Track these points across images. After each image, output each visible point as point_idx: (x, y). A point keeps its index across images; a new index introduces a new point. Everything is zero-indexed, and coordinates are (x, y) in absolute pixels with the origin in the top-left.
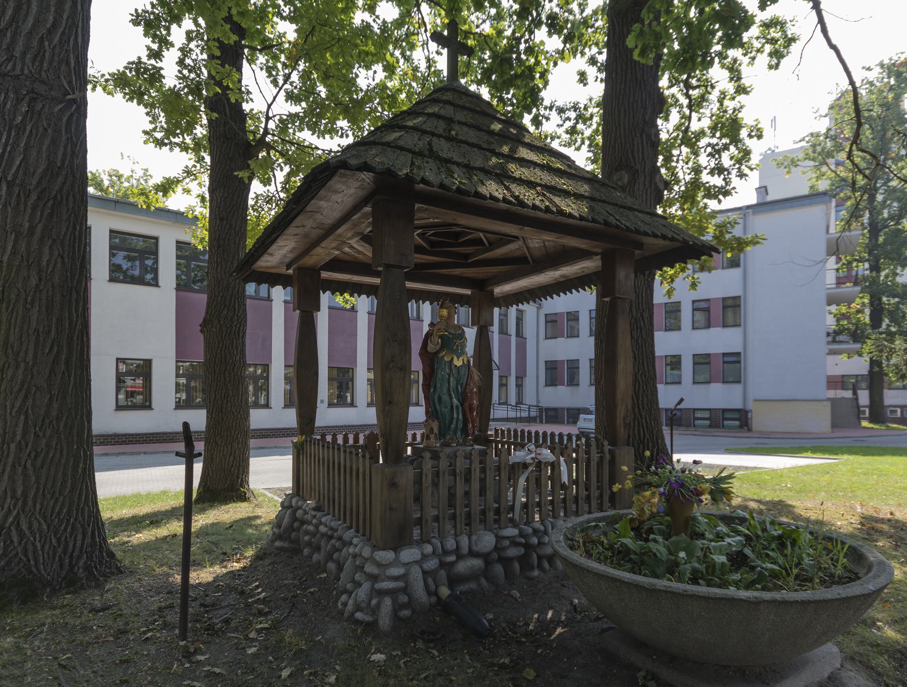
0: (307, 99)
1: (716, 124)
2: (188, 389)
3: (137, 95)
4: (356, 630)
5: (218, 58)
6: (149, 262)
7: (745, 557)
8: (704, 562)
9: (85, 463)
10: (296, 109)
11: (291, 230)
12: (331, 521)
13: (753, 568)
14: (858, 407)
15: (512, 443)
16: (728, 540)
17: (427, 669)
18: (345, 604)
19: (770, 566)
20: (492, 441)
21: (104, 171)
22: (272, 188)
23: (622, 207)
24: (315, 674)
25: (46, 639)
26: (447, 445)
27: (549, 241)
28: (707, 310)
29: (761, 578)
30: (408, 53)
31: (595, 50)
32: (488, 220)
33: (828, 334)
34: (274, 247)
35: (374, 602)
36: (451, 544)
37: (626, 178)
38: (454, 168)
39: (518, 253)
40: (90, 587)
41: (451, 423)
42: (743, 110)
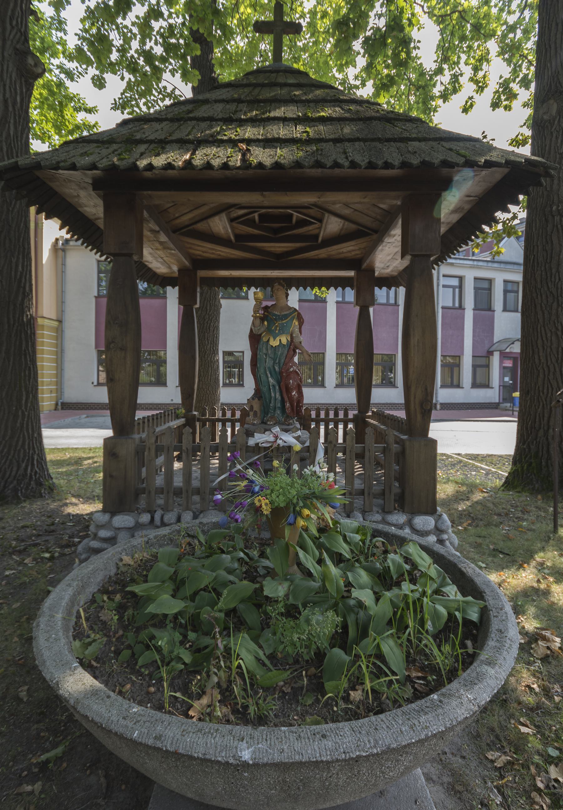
41: (270, 402)
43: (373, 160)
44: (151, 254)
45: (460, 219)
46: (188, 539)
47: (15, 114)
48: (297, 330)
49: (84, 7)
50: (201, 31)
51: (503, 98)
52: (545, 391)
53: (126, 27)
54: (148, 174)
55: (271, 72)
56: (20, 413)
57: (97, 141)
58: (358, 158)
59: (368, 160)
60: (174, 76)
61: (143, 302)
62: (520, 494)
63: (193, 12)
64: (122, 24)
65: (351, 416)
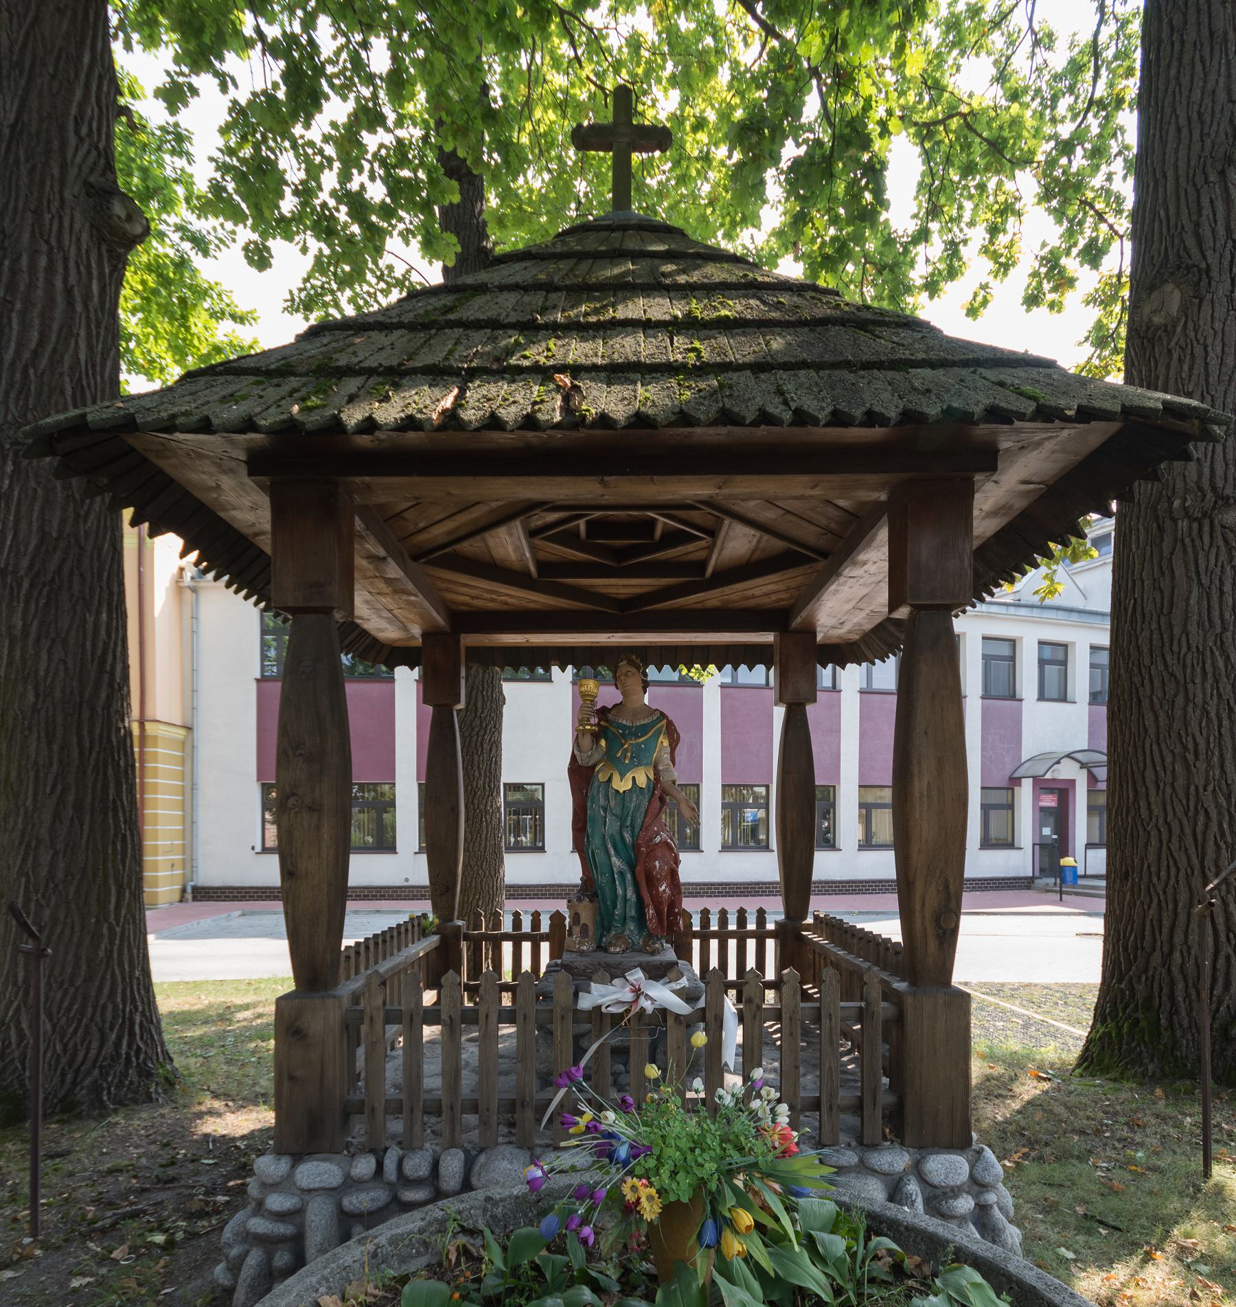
32: (754, 478)
41: (615, 907)
43: (843, 406)
44: (367, 602)
45: (1002, 529)
46: (462, 1240)
47: (88, 317)
48: (667, 756)
49: (224, 102)
50: (461, 153)
51: (1047, 286)
52: (1163, 874)
53: (311, 144)
54: (364, 440)
55: (610, 228)
56: (105, 930)
57: (255, 371)
58: (809, 404)
59: (830, 409)
60: (407, 244)
61: (351, 689)
62: (1117, 1085)
63: (443, 115)
64: (302, 137)
65: (770, 926)
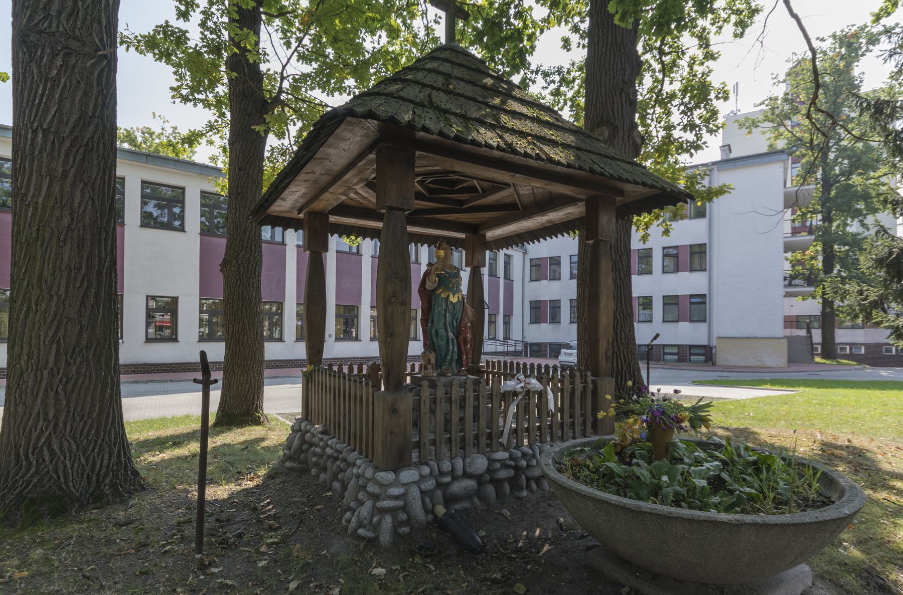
0: (316, 60)
1: (686, 87)
2: (210, 324)
3: (165, 56)
4: (359, 545)
5: (237, 21)
6: (177, 210)
7: (724, 481)
8: (685, 486)
9: (112, 389)
10: (307, 69)
11: (302, 176)
12: (337, 443)
13: (731, 492)
14: (812, 344)
15: (502, 374)
16: (707, 465)
17: (424, 583)
18: (349, 521)
19: (748, 490)
20: (483, 372)
21: (138, 129)
22: (286, 142)
23: (605, 156)
24: (320, 587)
25: (73, 551)
26: (443, 374)
27: (538, 188)
28: (676, 256)
29: (739, 502)
30: (409, 21)
31: (577, 19)
32: (481, 167)
33: (785, 279)
34: (286, 192)
35: (375, 519)
36: (446, 466)
37: (606, 134)
38: (453, 119)
39: (509, 200)
40: (115, 503)
41: (447, 355)
42: (712, 74)
